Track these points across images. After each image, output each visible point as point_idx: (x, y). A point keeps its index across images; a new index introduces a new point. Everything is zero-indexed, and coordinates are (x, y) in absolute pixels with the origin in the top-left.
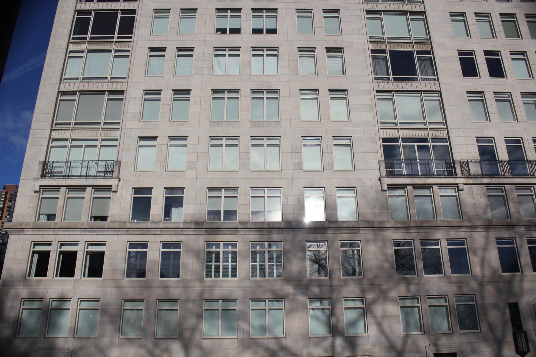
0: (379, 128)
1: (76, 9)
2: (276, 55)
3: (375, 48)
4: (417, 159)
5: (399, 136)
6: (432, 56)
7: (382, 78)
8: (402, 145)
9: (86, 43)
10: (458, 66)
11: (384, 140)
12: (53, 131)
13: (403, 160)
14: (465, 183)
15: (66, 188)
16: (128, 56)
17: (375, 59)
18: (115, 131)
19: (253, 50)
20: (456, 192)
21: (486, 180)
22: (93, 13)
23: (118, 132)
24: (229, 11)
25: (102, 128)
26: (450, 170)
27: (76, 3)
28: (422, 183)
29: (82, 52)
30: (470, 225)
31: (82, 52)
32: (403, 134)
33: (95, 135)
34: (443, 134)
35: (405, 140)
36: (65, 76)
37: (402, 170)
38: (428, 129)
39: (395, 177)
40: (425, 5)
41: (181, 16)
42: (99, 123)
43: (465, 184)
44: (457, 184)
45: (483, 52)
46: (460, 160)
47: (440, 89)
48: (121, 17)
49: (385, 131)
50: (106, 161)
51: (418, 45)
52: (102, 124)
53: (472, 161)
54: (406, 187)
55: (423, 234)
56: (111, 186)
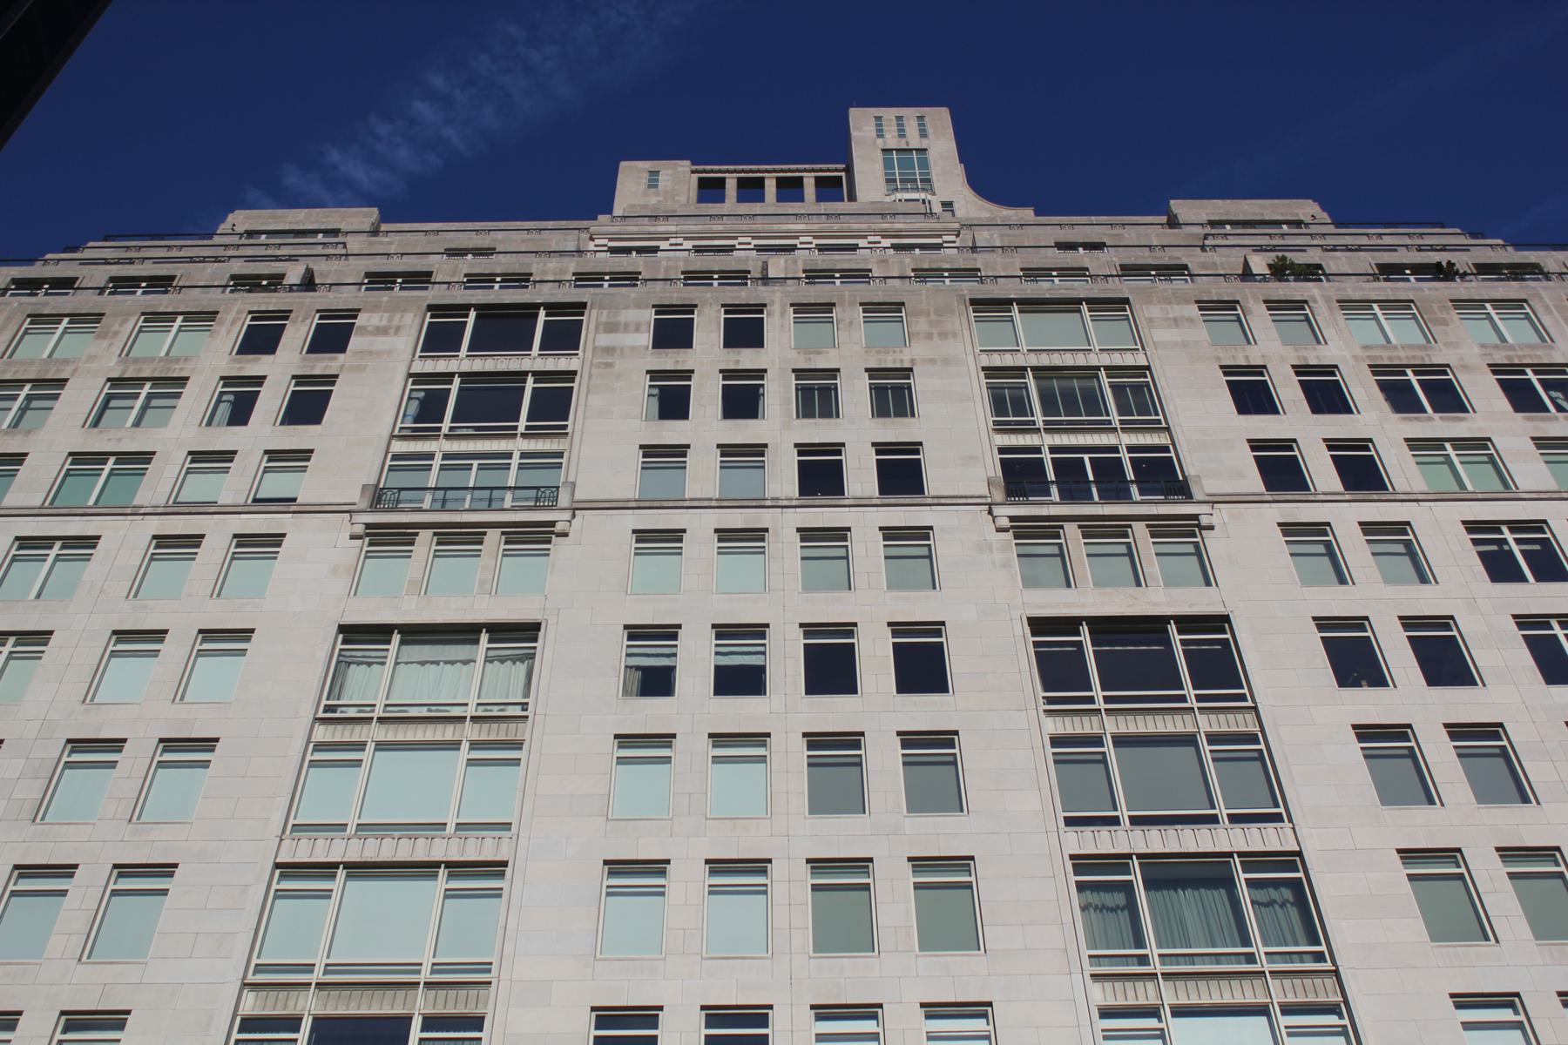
1: (277, 861)
4: (1135, 486)
6: (1262, 746)
9: (437, 440)
12: (246, 991)
15: (432, 534)
16: (517, 762)
22: (457, 380)
25: (427, 980)
27: (278, 839)
29: (360, 746)
31: (360, 746)
36: (295, 818)
37: (1027, 380)
45: (1315, 637)
47: (1299, 845)
48: (534, 388)
50: (538, 488)
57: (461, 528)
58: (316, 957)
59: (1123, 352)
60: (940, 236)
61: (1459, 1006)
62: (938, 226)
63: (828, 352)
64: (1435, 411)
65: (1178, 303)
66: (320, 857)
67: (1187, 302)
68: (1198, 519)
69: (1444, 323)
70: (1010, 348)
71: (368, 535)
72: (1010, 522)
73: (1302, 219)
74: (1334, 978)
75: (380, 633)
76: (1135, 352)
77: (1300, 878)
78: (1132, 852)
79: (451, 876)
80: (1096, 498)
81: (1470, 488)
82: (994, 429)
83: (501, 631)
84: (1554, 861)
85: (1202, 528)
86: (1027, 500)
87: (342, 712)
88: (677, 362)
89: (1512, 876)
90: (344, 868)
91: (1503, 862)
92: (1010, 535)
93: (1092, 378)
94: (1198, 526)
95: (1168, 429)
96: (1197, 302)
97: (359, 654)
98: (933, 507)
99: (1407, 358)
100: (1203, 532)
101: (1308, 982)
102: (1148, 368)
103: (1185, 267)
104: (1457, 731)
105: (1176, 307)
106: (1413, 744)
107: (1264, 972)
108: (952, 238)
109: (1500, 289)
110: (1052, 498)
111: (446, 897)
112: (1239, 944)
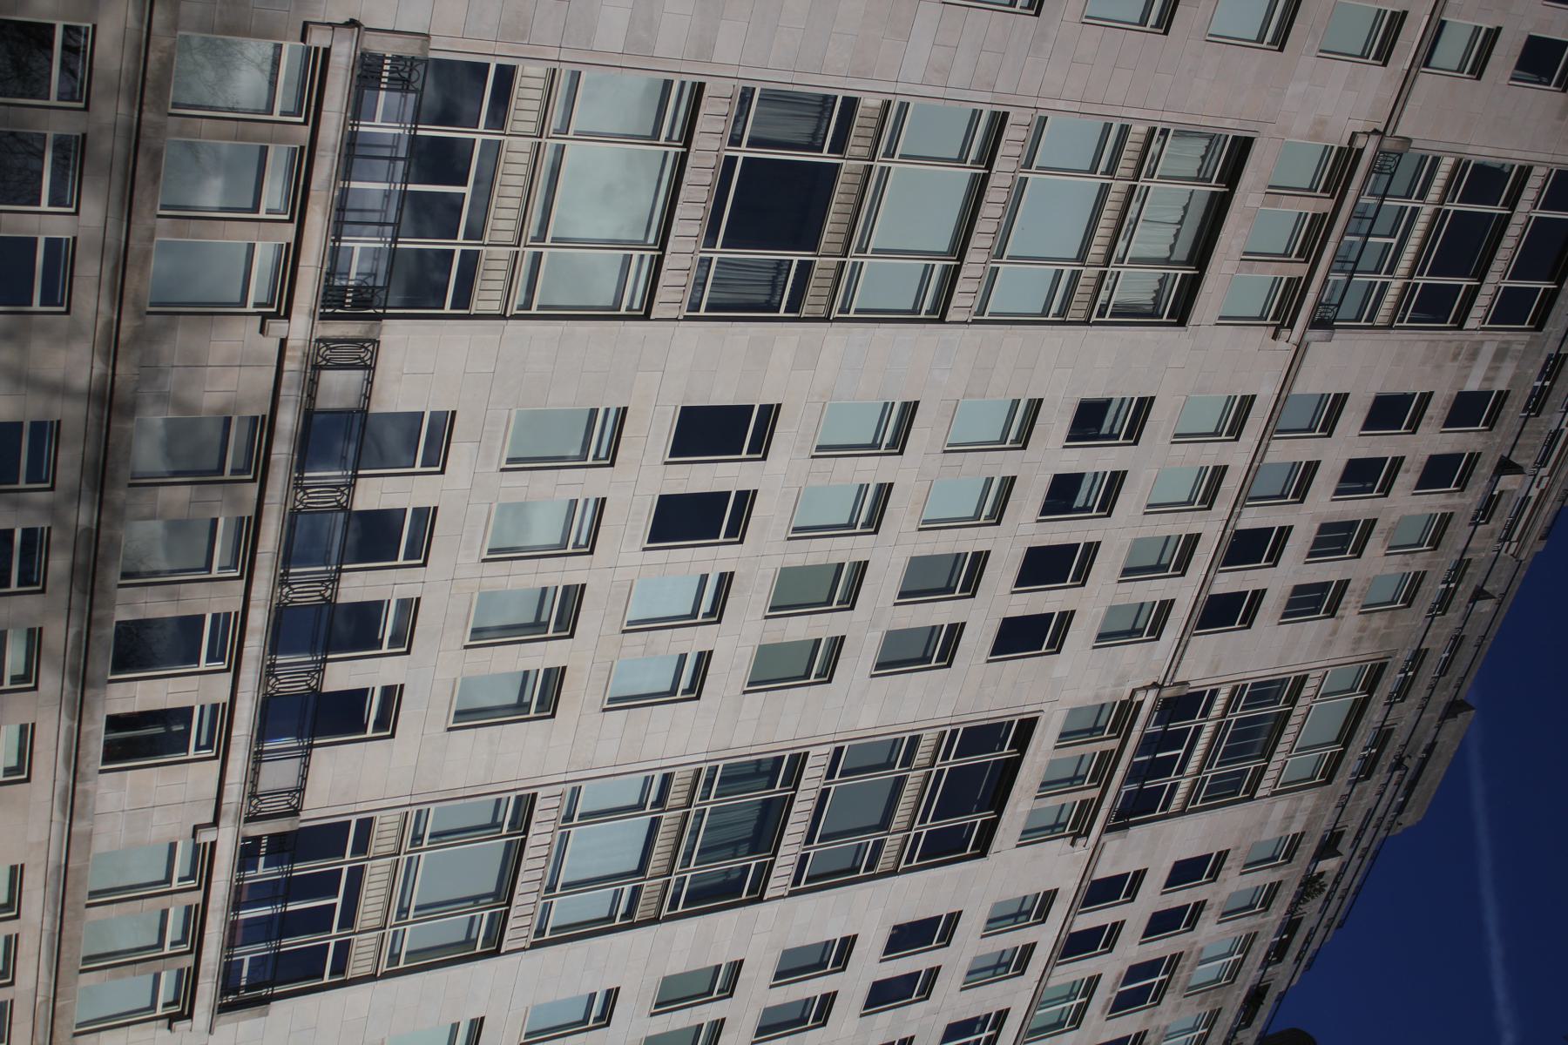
0: (556, 65)
5: (488, 245)
8: (474, 140)
11: (506, 75)
13: (416, 129)
14: (290, 343)
17: (774, 268)
20: (256, 305)
26: (383, 80)
28: (313, 186)
30: (122, 336)
32: (516, 150)
34: (486, 297)
38: (539, 140)
44: (288, 316)
46: (379, 342)
49: (540, 83)
53: (370, 382)
54: (306, 123)
55: (108, 146)
57: (1322, 239)
59: (1518, 239)
60: (1518, 540)
61: (722, 576)
62: (1530, 541)
63: (1383, 547)
64: (1119, 993)
65: (1308, 819)
67: (1307, 826)
68: (1287, 327)
69: (1201, 1003)
70: (1285, 771)
71: (1351, 149)
72: (1358, 149)
73: (1403, 815)
74: (499, 312)
75: (1232, 174)
76: (1482, 320)
77: (443, 308)
78: (993, 171)
80: (1136, 760)
81: (1038, 1013)
82: (1461, 160)
84: (821, 673)
85: (1278, 328)
86: (1155, 711)
87: (1159, 139)
88: (1431, 418)
89: (818, 642)
91: (832, 638)
92: (1345, 144)
93: (1263, 751)
94: (1282, 325)
95: (1390, 327)
96: (1303, 833)
97: (1218, 150)
98: (1177, 641)
99: (1179, 977)
100: (1274, 328)
101: (829, 283)
102: (1460, 327)
103: (1368, 777)
104: (980, 559)
105: (1305, 818)
106: (957, 593)
107: (846, 257)
108: (1512, 550)
109: (1217, 1040)
110: (1151, 727)
112: (723, 775)
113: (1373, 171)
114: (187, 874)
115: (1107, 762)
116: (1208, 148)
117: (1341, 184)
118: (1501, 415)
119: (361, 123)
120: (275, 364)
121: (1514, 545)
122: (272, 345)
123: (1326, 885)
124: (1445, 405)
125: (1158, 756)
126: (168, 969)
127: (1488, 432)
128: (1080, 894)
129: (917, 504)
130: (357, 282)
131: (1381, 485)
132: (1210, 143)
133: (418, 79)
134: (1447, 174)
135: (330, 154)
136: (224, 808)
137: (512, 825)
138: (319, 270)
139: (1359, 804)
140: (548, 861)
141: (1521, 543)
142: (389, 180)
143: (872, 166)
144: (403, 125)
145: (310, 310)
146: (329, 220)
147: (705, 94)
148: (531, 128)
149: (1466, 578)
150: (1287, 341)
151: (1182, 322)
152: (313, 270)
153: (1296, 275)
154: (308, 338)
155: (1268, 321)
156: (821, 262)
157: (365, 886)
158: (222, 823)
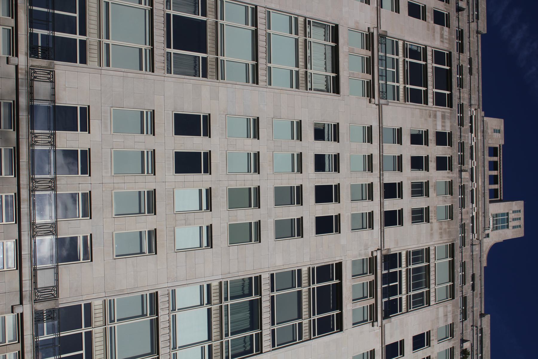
0: (105, 298)
2: (201, 208)
3: (214, 357)
7: (169, 3)
8: (82, 333)
10: (188, 109)
11: (88, 307)
13: (60, 334)
14: (19, 67)
15: (13, 26)
16: (292, 87)
17: (194, 5)
18: (96, 60)
19: (207, 190)
21: (23, 101)
23: (96, 64)
24: (255, 62)
26: (44, 312)
31: (297, 33)
32: (97, 332)
33: (92, 31)
35: (89, 335)
38: (105, 326)
39: (34, 354)
40: (270, 352)
41: (250, 119)
42: (108, 37)
43: (17, 67)
51: (219, 347)
52: (107, 41)
53: (54, 88)
54: (19, 342)
56: (17, 56)
58: (226, 21)
60: (477, 233)
62: (480, 232)
65: (453, 317)
66: (259, 21)
67: (453, 320)
68: (376, 321)
71: (369, 33)
72: (375, 256)
75: (336, 39)
76: (435, 301)
79: (253, 65)
80: (383, 286)
82: (407, 251)
83: (336, 81)
87: (308, 27)
88: (431, 140)
90: (255, 29)
92: (370, 256)
93: (426, 285)
95: (407, 312)
96: (453, 323)
97: (328, 32)
100: (372, 323)
102: (429, 305)
103: (466, 319)
108: (476, 237)
111: (246, 64)
113: (379, 43)
114: (12, 339)
115: (373, 285)
116: (325, 32)
117: (371, 46)
118: (452, 141)
119: (39, 337)
120: (15, 78)
121: (476, 235)
122: (12, 68)
123: (469, 352)
124: (434, 135)
125: (390, 285)
126: (11, 351)
127: (452, 339)
128: (383, 351)
129: (270, 162)
130: (47, 313)
131: (426, 302)
132: (325, 30)
133: (57, 316)
134: (406, 299)
135: (30, 353)
136: (24, 293)
137: (151, 314)
138: (26, 36)
139: (467, 332)
140: (170, 329)
141: (478, 233)
142: (52, 263)
143: (222, 305)
144: (55, 334)
145: (26, 53)
146: (27, 16)
147: (159, 295)
148: (101, 323)
149: (466, 231)
150: (377, 326)
151: (341, 330)
152: (24, 36)
153: (372, 303)
154: (27, 65)
155: (369, 321)
156: (215, 343)
157: (94, 340)
158: (24, 302)
